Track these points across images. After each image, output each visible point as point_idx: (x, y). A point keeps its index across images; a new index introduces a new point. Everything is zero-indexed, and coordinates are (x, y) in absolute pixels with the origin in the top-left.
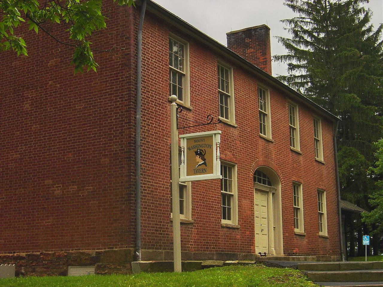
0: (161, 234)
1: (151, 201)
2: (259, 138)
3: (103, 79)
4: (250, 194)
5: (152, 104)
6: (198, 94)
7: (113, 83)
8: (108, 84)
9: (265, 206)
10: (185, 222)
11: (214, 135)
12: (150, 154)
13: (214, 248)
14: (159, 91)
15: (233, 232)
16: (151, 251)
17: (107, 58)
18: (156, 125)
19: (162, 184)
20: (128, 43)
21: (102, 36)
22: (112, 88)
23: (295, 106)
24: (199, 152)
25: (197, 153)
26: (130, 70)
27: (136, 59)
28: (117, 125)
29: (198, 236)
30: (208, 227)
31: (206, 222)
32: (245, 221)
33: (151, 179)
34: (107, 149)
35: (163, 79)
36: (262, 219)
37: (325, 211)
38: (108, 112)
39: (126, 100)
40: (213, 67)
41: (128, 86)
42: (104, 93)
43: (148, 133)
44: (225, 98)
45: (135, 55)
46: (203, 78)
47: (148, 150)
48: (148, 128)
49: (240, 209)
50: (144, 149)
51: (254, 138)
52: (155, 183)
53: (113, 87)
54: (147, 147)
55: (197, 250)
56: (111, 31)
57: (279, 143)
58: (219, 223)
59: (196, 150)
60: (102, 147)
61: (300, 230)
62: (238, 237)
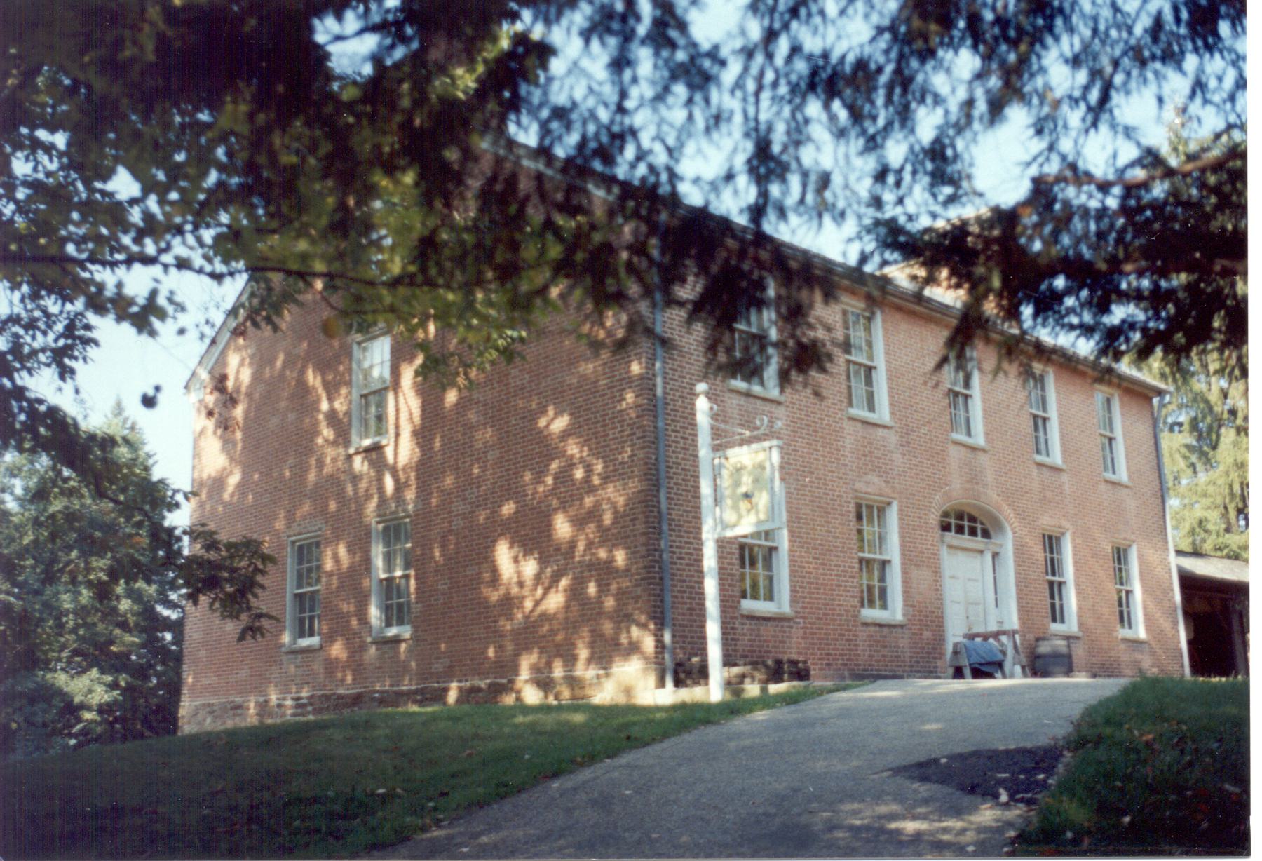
9: (976, 580)
44: (1039, 422)
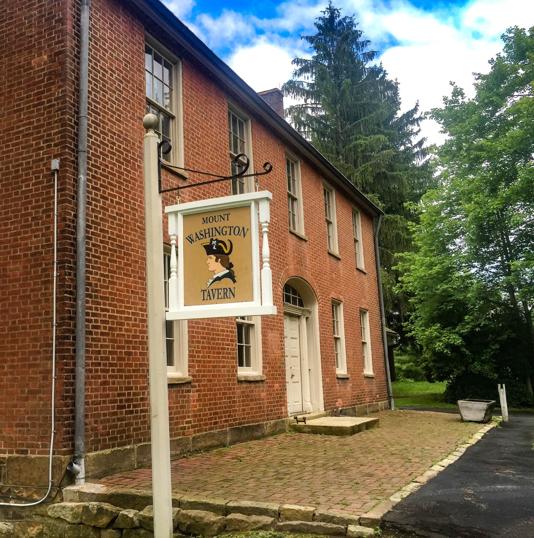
0: (131, 412)
1: (110, 349)
2: (289, 234)
3: (14, 107)
4: (278, 323)
5: (112, 158)
6: (197, 153)
7: (33, 112)
8: (22, 117)
9: (296, 339)
10: (176, 383)
11: (253, 205)
12: (107, 254)
13: (226, 421)
14: (127, 135)
15: (256, 387)
16: (108, 451)
17: (21, 64)
18: (120, 198)
19: (133, 314)
20: (61, 31)
21: (11, 24)
22: (30, 123)
23: (331, 191)
24: (214, 248)
25: (209, 249)
26: (65, 84)
27: (79, 63)
28: (38, 195)
29: (200, 405)
30: (216, 385)
31: (214, 376)
32: (273, 367)
33: (110, 305)
34: (20, 245)
35: (133, 114)
36: (293, 358)
37: (367, 339)
38: (23, 170)
39: (55, 145)
40: (221, 112)
41: (60, 117)
42: (14, 134)
43: (104, 214)
45: (75, 56)
46: (205, 126)
47: (104, 248)
48: (104, 203)
49: (265, 348)
50: (94, 245)
51: (282, 233)
52: (118, 312)
53: (32, 120)
54: (102, 242)
55: (199, 431)
56: (28, 11)
57: (314, 242)
58: (234, 375)
59: (207, 241)
60: (10, 241)
61: (342, 371)
62: (263, 394)
